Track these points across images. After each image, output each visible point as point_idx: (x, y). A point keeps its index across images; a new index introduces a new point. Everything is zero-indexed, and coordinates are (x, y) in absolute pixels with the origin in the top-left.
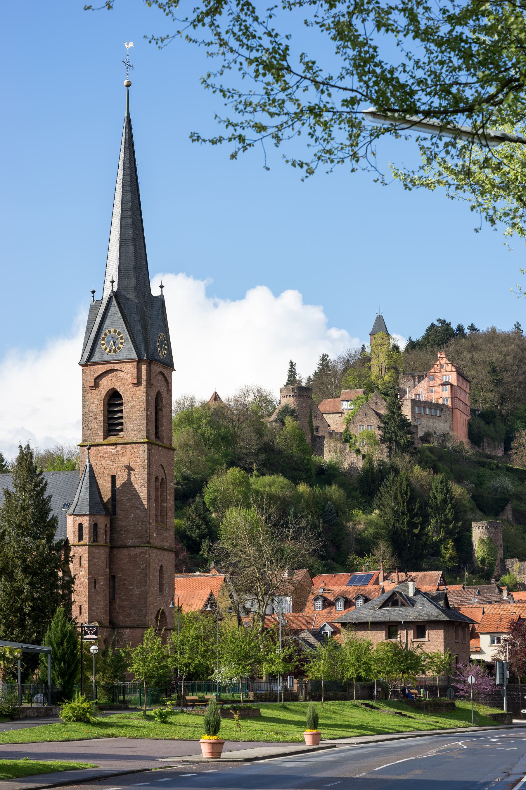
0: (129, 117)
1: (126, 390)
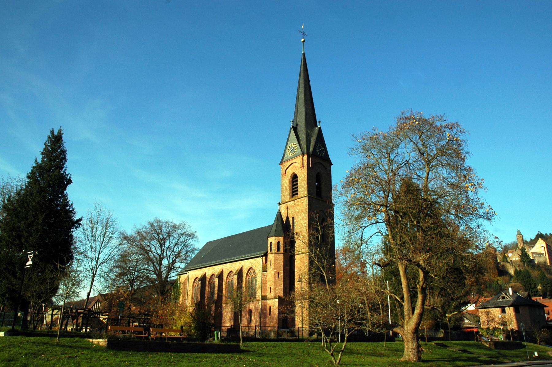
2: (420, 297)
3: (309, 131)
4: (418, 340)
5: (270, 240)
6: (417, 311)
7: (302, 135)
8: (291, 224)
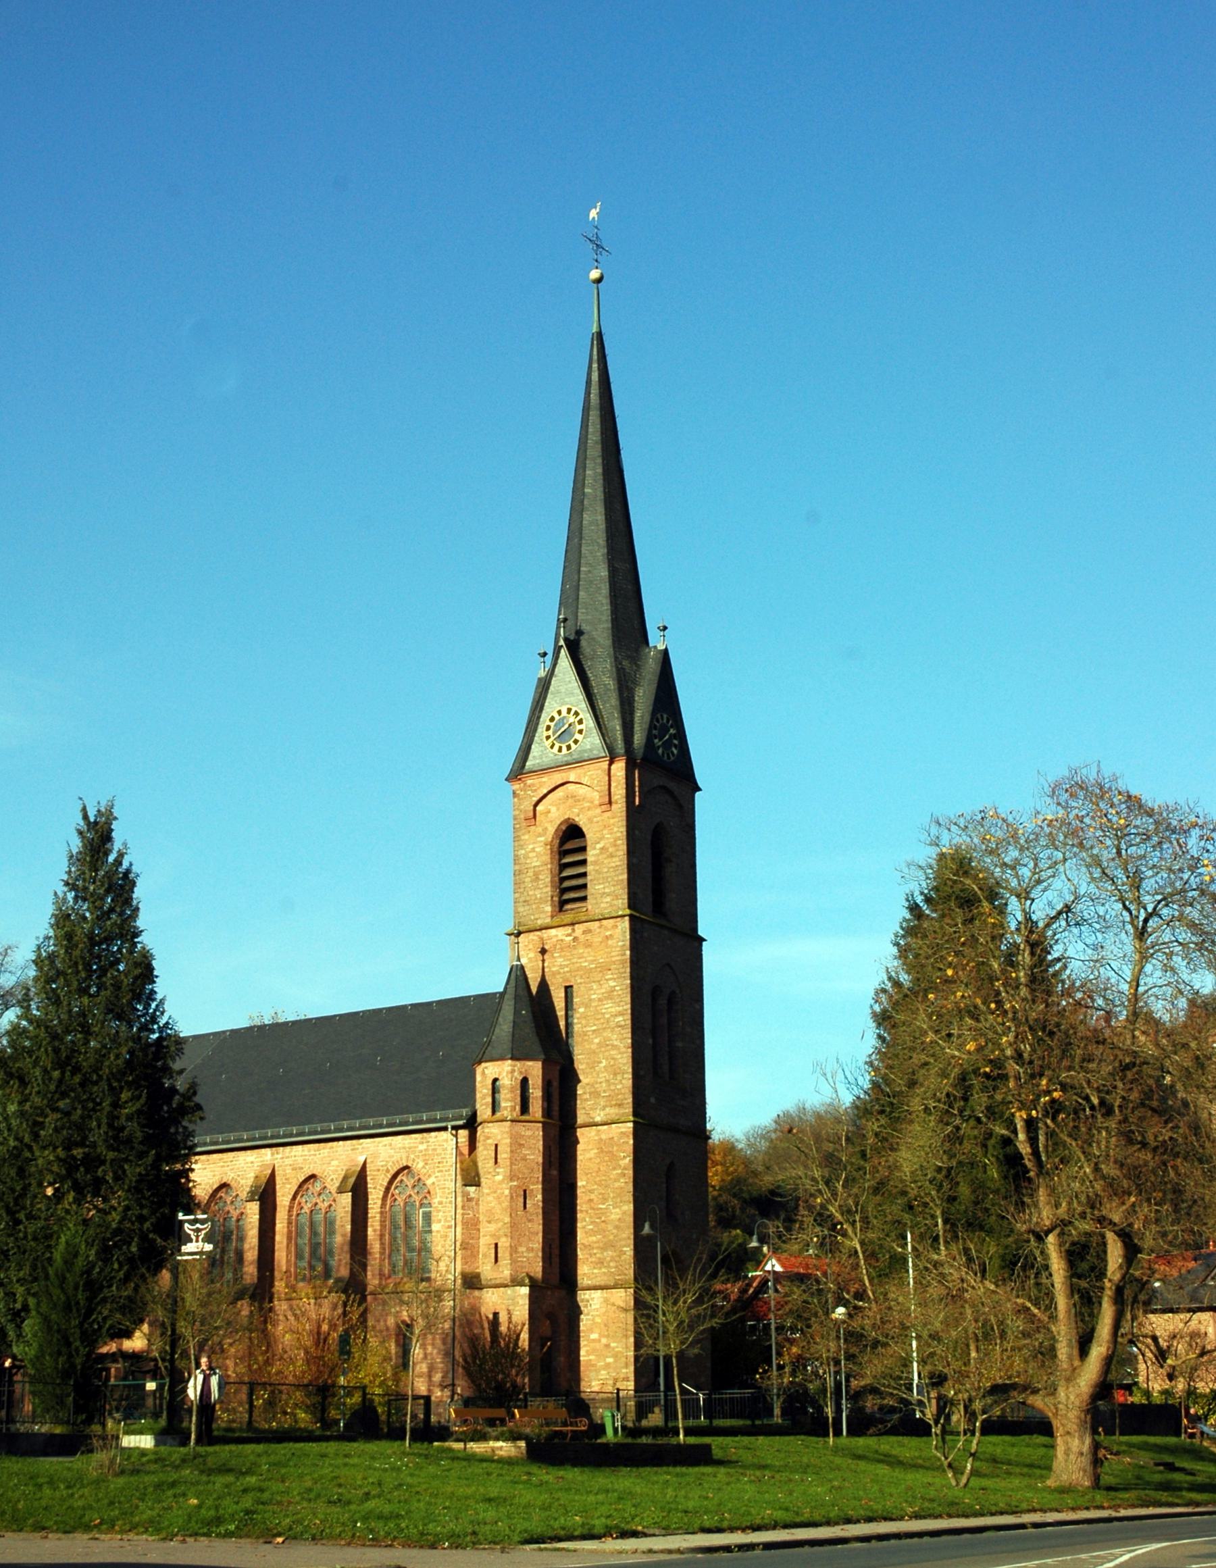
0: (600, 335)
1: (590, 820)
2: (1107, 1312)
3: (625, 663)
4: (1094, 1432)
5: (487, 1072)
6: (1098, 1351)
7: (604, 680)
8: (561, 1013)
